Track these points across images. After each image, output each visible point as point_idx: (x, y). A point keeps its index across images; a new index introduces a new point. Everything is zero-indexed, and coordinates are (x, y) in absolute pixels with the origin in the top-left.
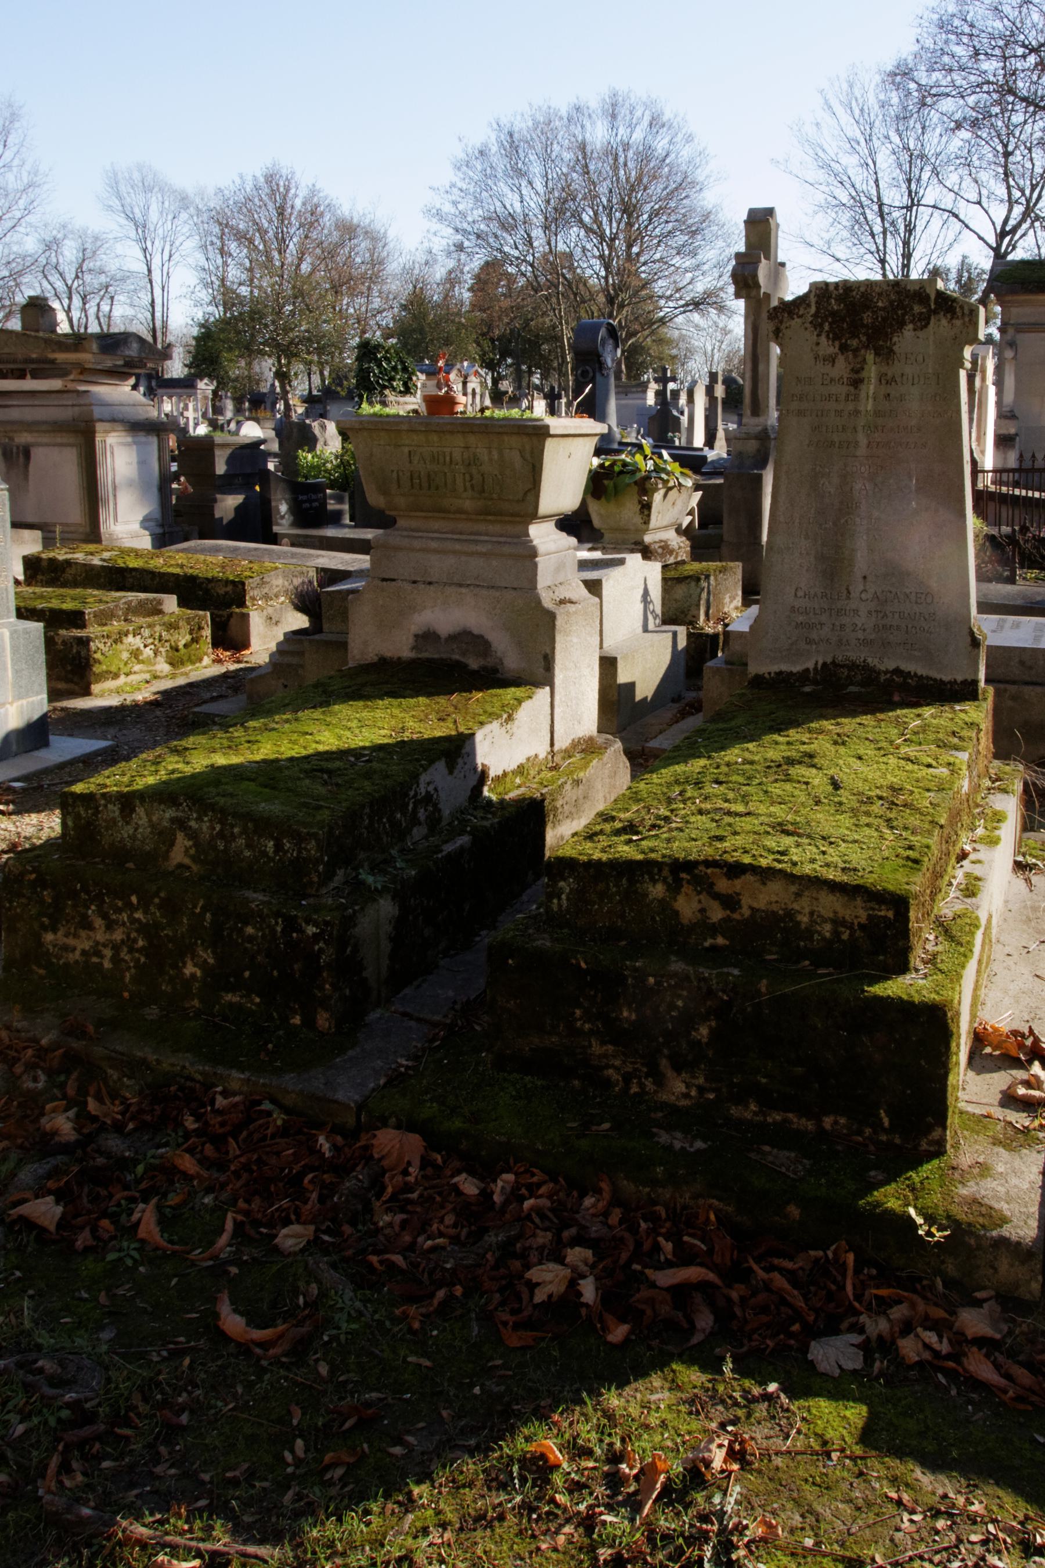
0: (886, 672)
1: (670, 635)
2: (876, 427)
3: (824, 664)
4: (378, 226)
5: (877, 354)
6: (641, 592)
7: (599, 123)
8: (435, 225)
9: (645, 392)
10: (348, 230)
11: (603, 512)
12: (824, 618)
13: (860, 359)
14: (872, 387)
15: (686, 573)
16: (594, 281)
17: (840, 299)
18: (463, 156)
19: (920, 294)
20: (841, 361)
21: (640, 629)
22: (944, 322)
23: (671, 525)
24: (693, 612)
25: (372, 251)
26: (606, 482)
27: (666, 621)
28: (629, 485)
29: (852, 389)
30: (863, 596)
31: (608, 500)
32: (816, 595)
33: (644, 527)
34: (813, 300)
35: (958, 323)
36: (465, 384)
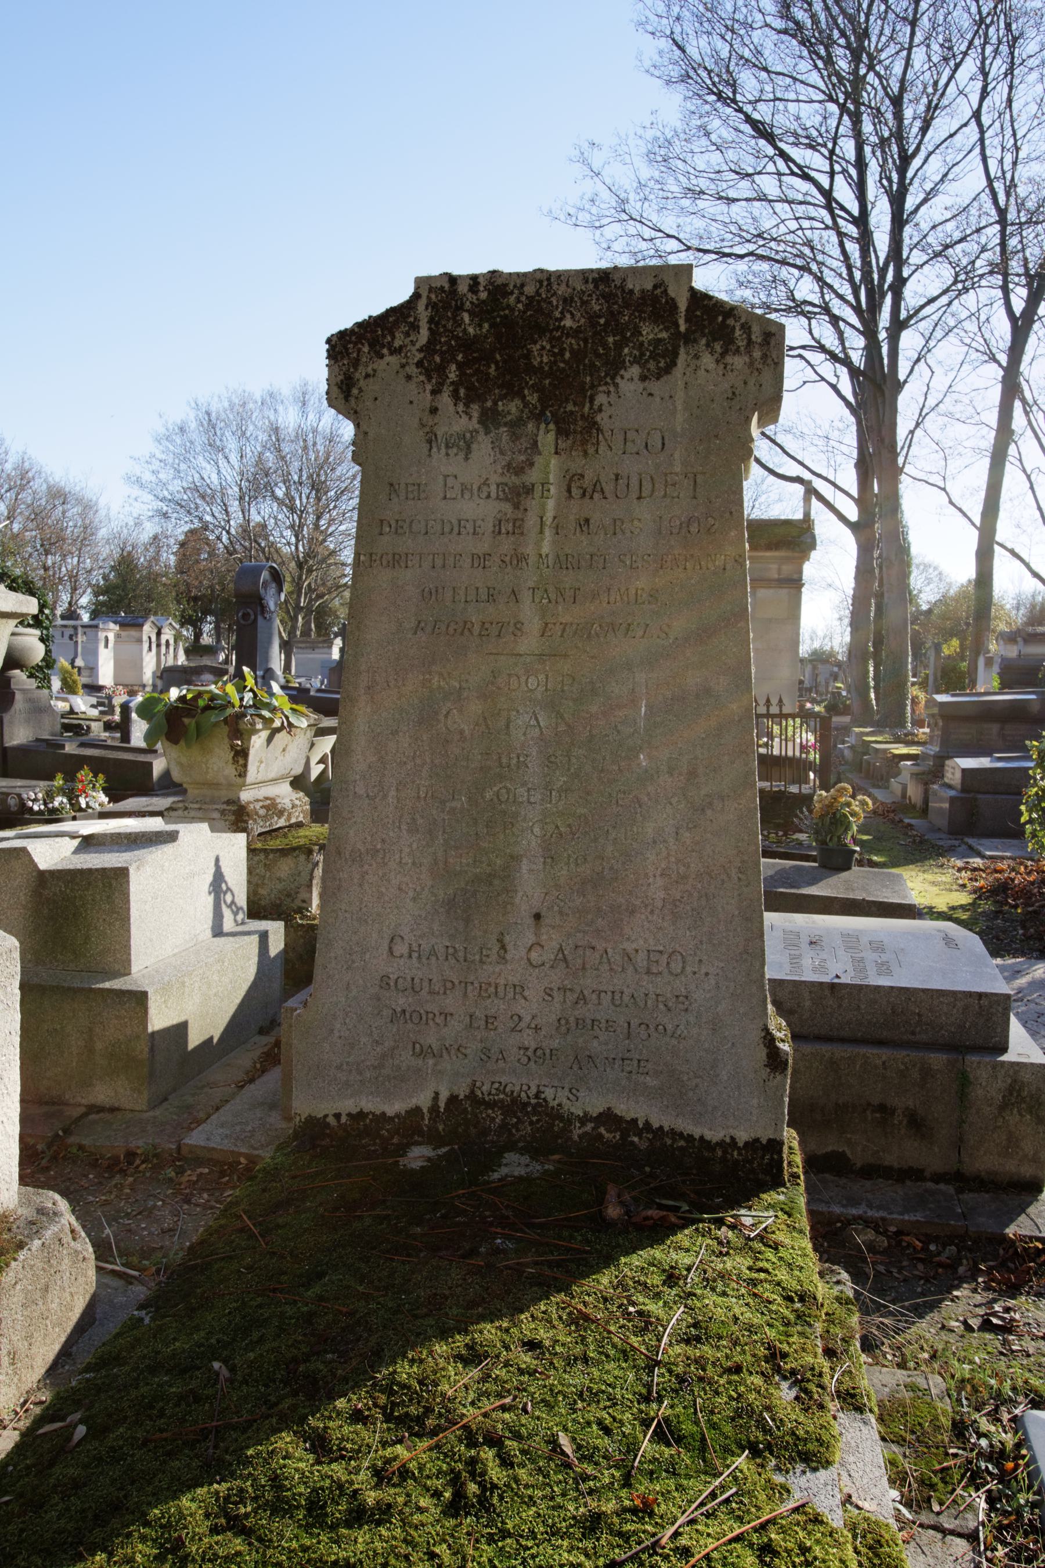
0: (585, 1119)
1: (255, 938)
2: (560, 592)
3: (453, 1099)
4: (89, 495)
5: (562, 432)
6: (209, 878)
7: (291, 409)
8: (136, 491)
9: (330, 647)
10: (59, 495)
11: (184, 760)
12: (451, 1002)
13: (524, 443)
14: (551, 504)
15: (295, 843)
16: (286, 550)
17: (480, 312)
18: (163, 430)
19: (655, 300)
20: (483, 447)
21: (209, 933)
22: (707, 360)
23: (282, 778)
24: (303, 895)
25: (83, 515)
26: (186, 721)
27: (256, 910)
28: (216, 725)
29: (507, 507)
30: (534, 955)
31: (189, 746)
32: (433, 952)
33: (239, 780)
34: (423, 313)
35: (738, 362)
36: (159, 634)
